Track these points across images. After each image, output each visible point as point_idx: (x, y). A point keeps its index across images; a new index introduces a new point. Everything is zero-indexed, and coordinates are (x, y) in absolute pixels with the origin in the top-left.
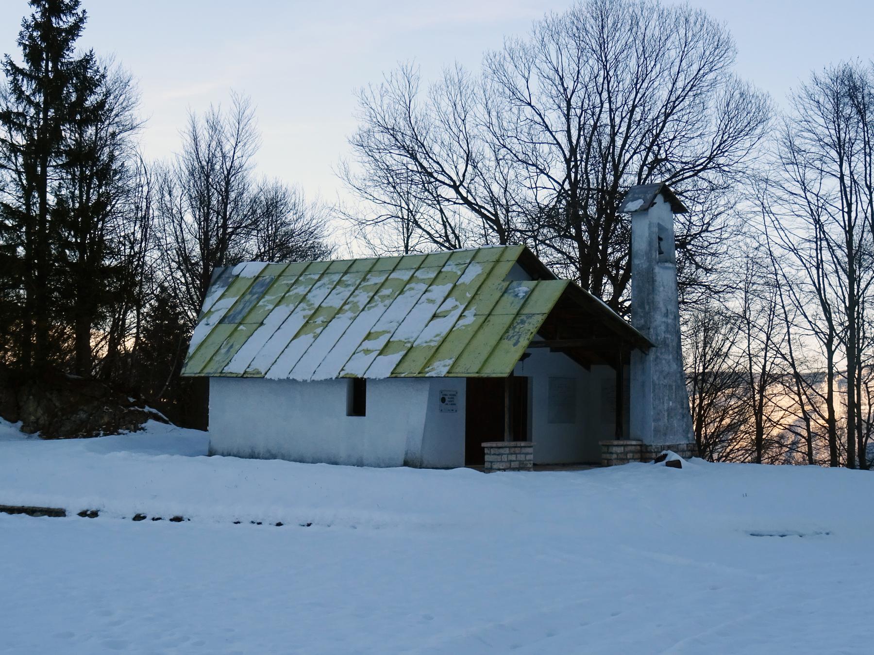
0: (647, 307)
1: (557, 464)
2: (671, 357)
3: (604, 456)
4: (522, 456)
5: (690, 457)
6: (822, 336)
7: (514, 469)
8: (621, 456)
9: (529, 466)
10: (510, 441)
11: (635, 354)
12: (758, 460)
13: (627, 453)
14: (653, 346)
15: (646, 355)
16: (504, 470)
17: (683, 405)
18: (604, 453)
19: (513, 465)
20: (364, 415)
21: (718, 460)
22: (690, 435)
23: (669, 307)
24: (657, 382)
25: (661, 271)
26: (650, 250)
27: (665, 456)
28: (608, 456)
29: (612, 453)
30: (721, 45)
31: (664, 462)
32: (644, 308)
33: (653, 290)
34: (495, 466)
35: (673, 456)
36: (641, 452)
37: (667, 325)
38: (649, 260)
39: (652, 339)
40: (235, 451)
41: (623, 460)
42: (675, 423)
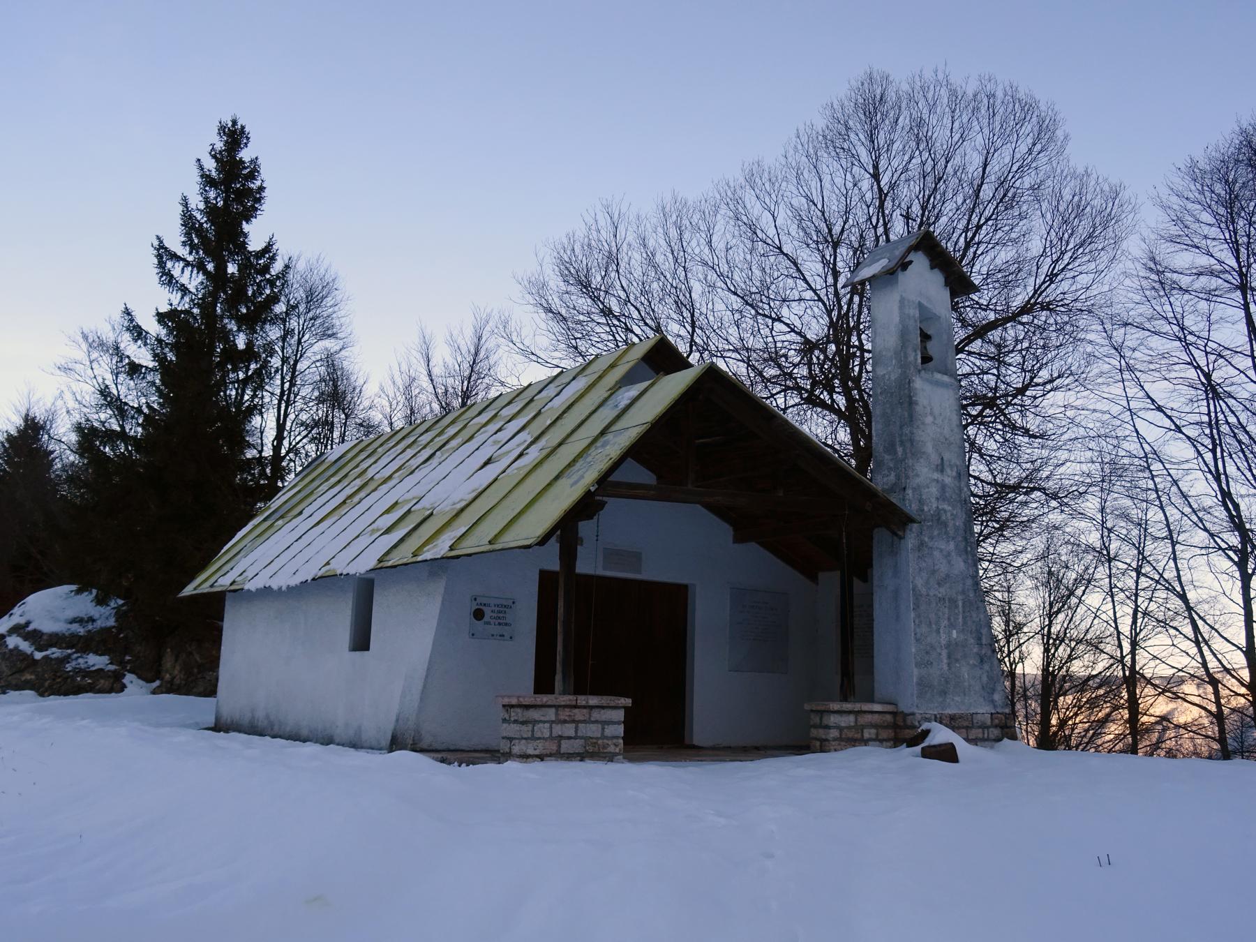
0: (900, 450)
1: (757, 748)
2: (952, 546)
3: (814, 732)
4: (593, 727)
5: (1000, 740)
6: (1231, 553)
7: (569, 757)
8: (851, 734)
9: (612, 749)
10: (564, 693)
11: (881, 536)
12: (1133, 749)
13: (863, 727)
14: (913, 521)
15: (901, 538)
16: (541, 758)
17: (980, 639)
18: (815, 726)
19: (566, 746)
20: (368, 649)
21: (1077, 747)
22: (997, 697)
23: (946, 456)
24: (924, 591)
25: (928, 387)
26: (904, 346)
27: (926, 733)
28: (821, 733)
29: (827, 727)
30: (1045, 132)
31: (918, 749)
32: (896, 453)
33: (912, 417)
34: (516, 749)
35: (941, 735)
36: (895, 726)
37: (943, 488)
38: (904, 365)
39: (911, 508)
40: (246, 721)
41: (853, 740)
42: (965, 672)
